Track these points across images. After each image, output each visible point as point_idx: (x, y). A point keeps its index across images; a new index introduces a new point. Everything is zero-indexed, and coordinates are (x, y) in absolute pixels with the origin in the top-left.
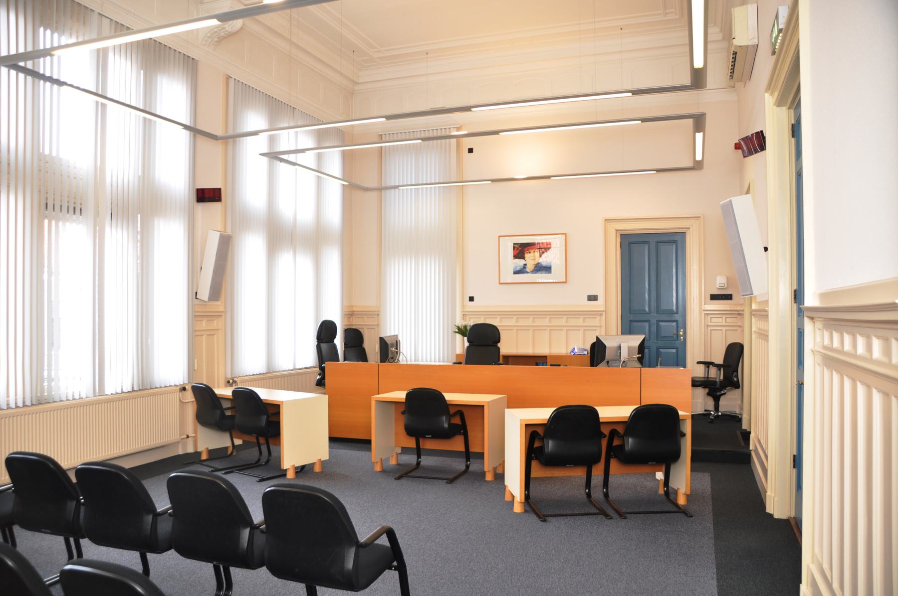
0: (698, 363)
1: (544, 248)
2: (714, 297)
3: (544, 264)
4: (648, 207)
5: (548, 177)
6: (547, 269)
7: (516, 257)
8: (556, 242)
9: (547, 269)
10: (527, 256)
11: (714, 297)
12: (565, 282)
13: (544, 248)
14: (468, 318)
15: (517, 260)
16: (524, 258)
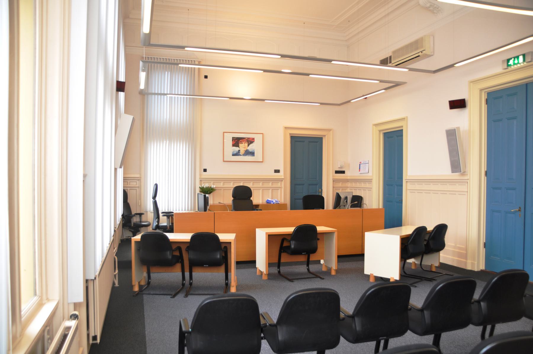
1: (250, 141)
2: (337, 172)
3: (250, 150)
4: (306, 122)
5: (264, 100)
6: (252, 154)
7: (233, 145)
8: (258, 139)
9: (252, 154)
10: (240, 145)
11: (337, 172)
13: (250, 141)
14: (203, 182)
15: (234, 148)
16: (238, 146)
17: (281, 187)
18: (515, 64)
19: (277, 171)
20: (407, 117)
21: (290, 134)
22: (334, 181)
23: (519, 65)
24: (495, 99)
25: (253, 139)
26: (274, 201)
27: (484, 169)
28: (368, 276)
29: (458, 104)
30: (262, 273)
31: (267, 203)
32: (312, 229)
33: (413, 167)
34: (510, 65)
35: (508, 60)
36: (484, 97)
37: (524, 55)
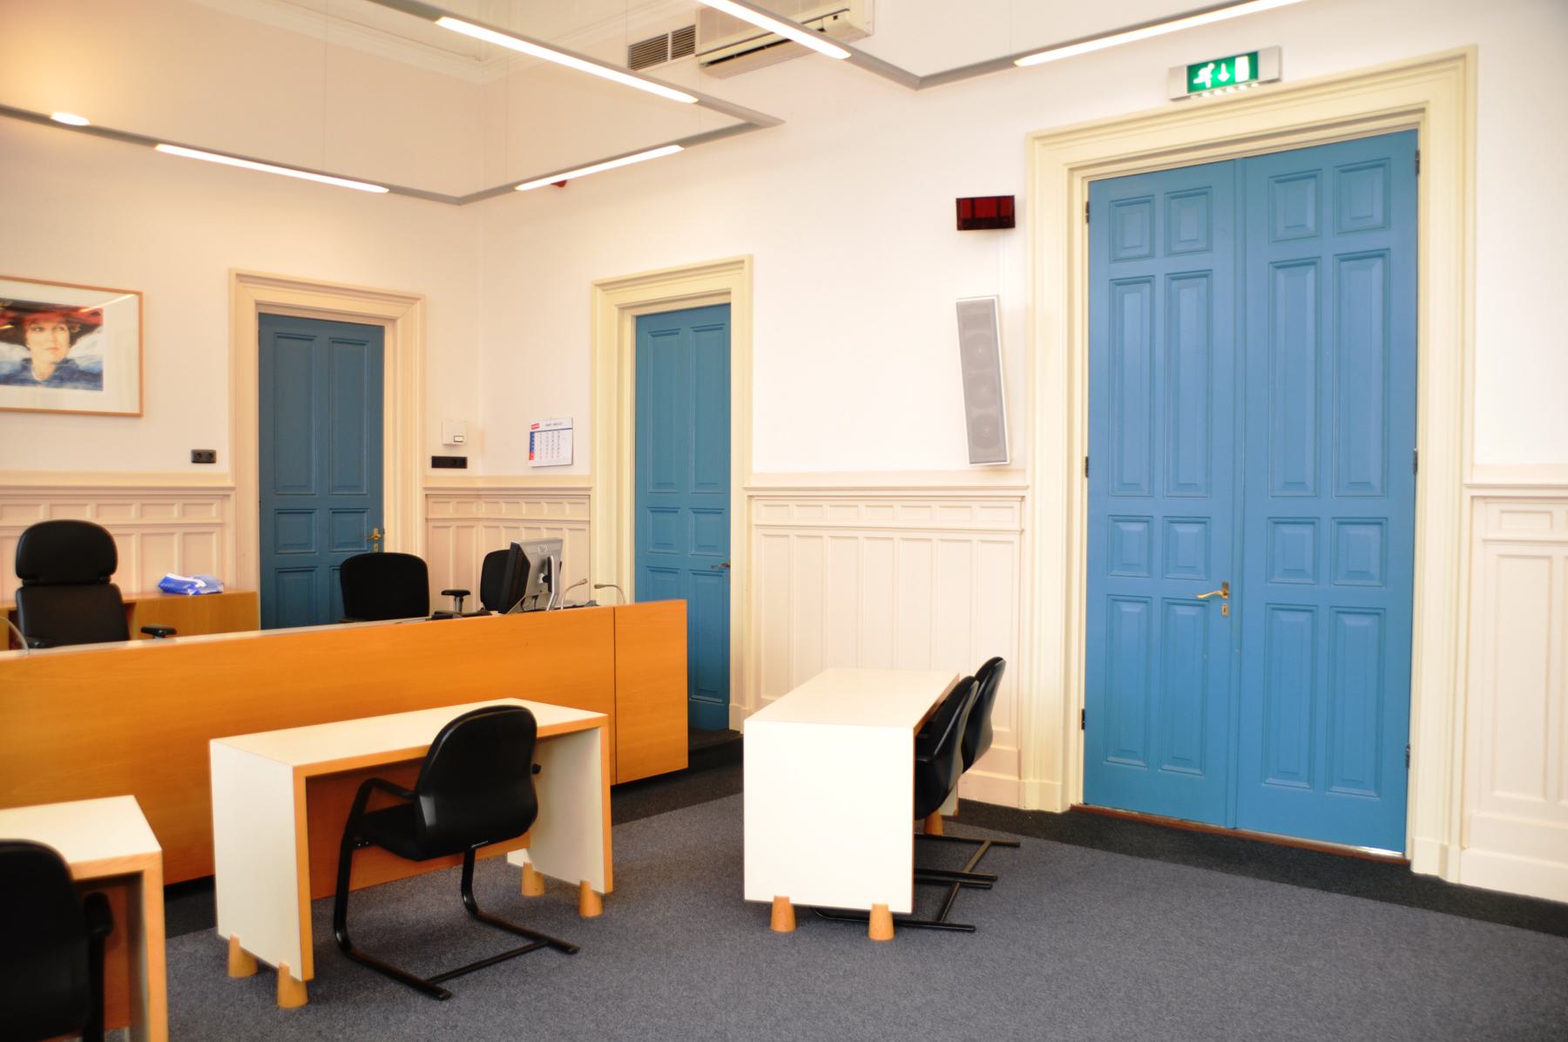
0: (444, 593)
1: (81, 324)
2: (438, 462)
3: (83, 364)
6: (91, 378)
8: (116, 312)
9: (91, 378)
10: (33, 337)
11: (438, 462)
12: (138, 416)
13: (81, 324)
17: (221, 525)
18: (1217, 84)
19: (204, 457)
20: (751, 257)
21: (258, 304)
22: (431, 495)
23: (1230, 89)
24: (1131, 208)
25: (96, 313)
26: (200, 584)
27: (1081, 451)
28: (764, 911)
29: (987, 214)
30: (265, 973)
31: (166, 590)
32: (523, 720)
33: (772, 437)
34: (1202, 87)
35: (1193, 70)
36: (1081, 196)
37: (1253, 57)
